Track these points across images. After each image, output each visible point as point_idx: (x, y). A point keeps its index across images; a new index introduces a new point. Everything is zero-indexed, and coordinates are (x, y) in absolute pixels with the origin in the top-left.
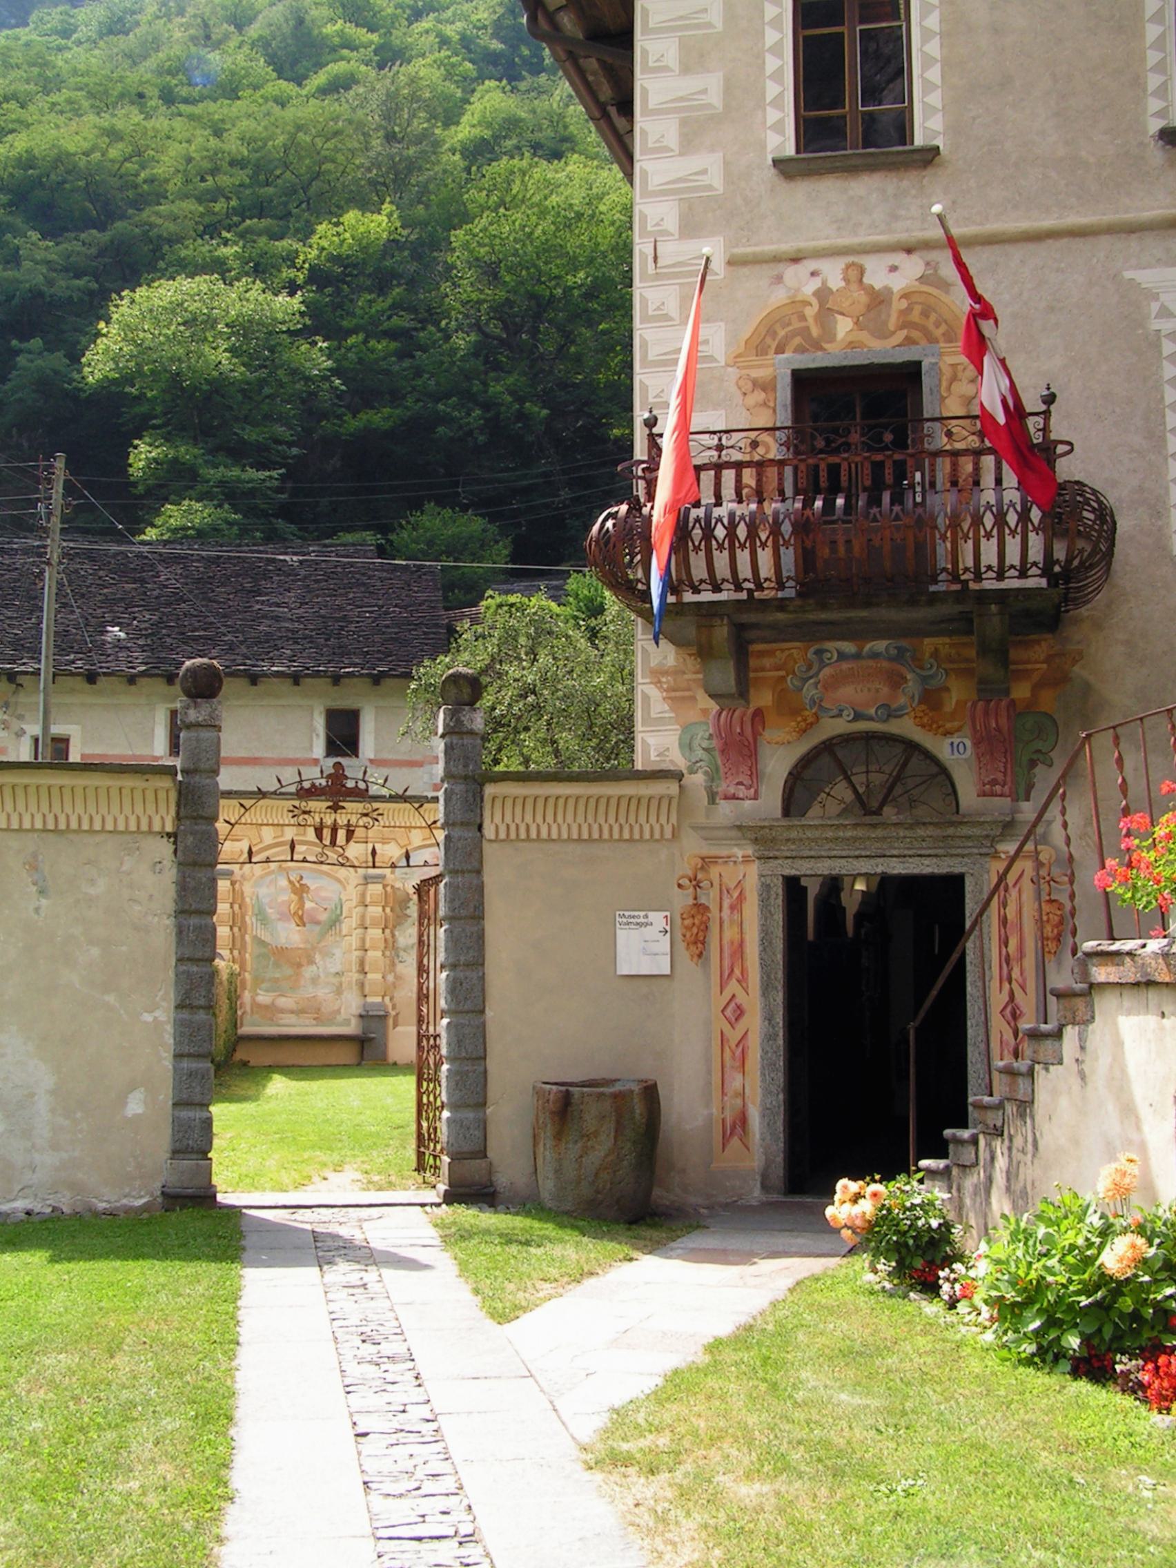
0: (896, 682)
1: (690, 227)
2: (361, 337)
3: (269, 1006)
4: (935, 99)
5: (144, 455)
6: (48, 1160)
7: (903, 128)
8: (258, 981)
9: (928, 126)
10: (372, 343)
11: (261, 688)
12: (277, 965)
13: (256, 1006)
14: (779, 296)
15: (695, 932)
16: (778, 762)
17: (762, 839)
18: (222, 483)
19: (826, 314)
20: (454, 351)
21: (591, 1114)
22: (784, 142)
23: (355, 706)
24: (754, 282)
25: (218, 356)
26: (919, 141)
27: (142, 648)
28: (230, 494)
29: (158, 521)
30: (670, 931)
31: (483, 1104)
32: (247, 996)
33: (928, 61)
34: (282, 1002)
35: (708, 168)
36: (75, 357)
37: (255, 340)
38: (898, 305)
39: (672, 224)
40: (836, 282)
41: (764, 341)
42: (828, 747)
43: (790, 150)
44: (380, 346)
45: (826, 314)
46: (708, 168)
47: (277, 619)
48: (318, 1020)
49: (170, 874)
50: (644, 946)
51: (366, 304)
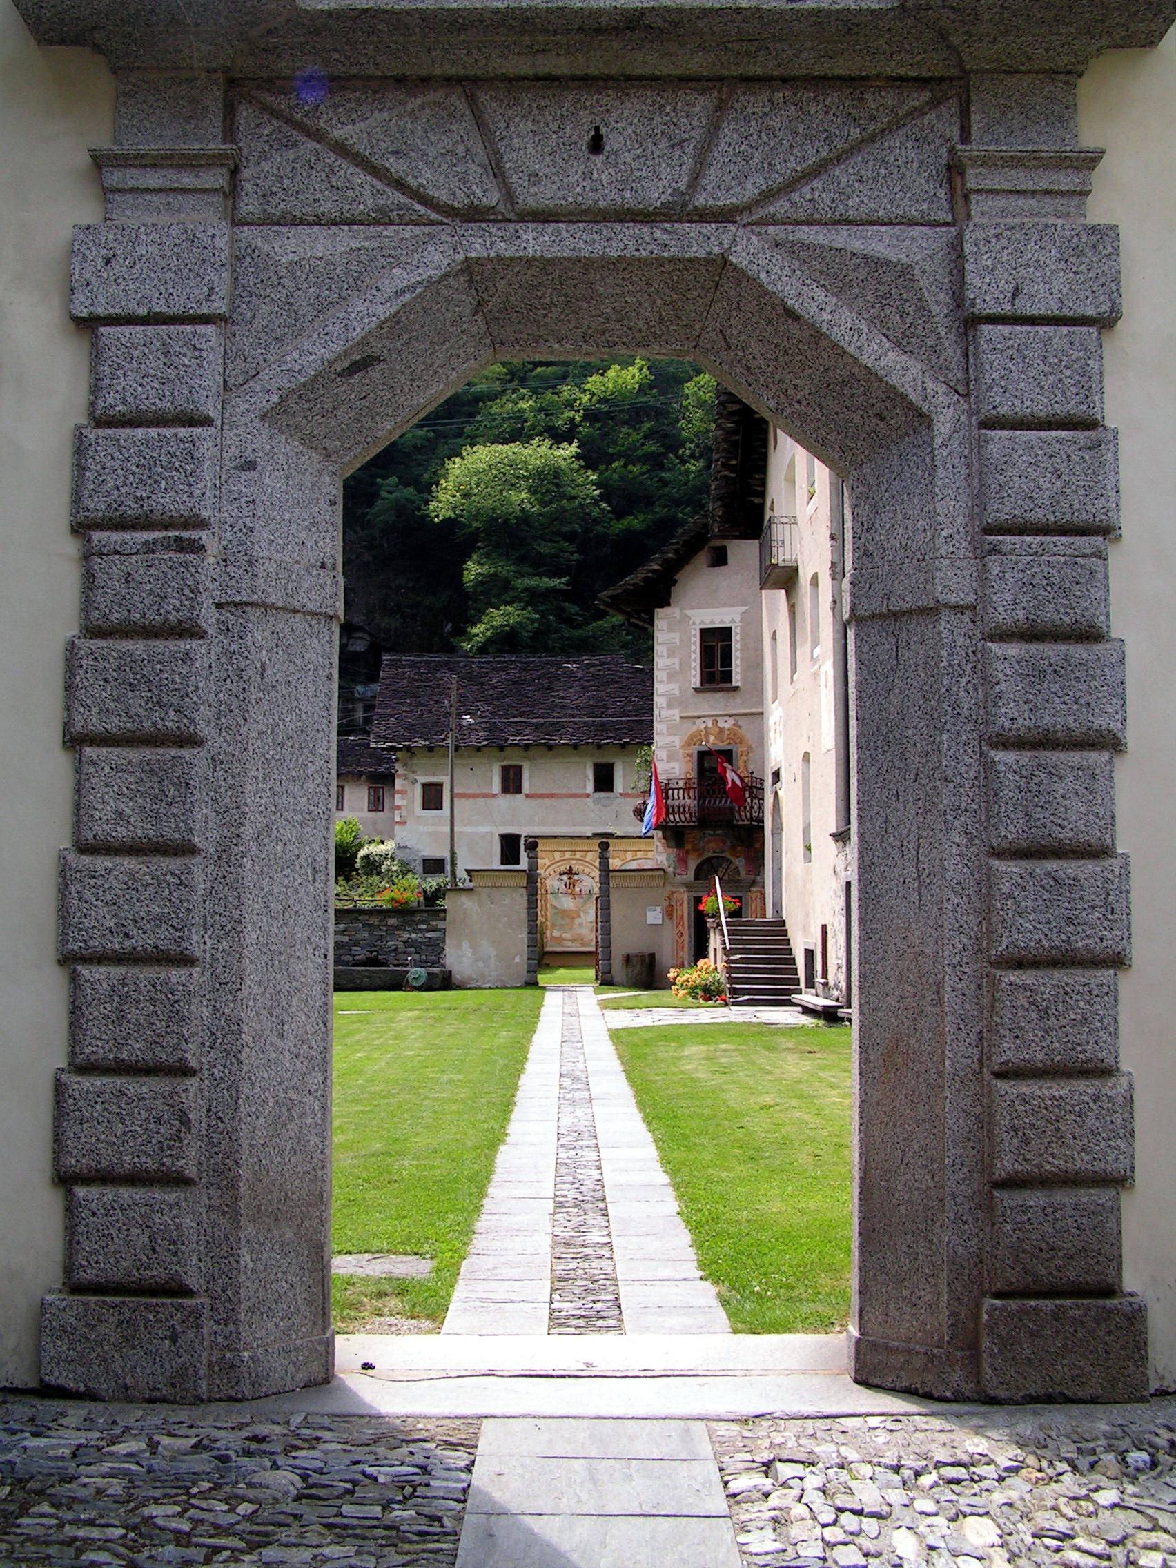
0: (724, 842)
1: (669, 707)
2: (622, 462)
3: (559, 937)
4: (738, 670)
5: (473, 570)
6: (494, 974)
7: (727, 677)
8: (553, 925)
9: (737, 680)
10: (630, 467)
11: (554, 752)
12: (562, 918)
13: (553, 937)
14: (694, 728)
15: (669, 912)
16: (692, 865)
17: (688, 886)
18: (526, 589)
19: (707, 735)
20: (687, 472)
21: (634, 961)
22: (696, 681)
23: (612, 761)
24: (688, 724)
25: (520, 498)
26: (734, 684)
27: (484, 730)
28: (534, 597)
29: (485, 619)
30: (662, 912)
31: (609, 959)
32: (548, 933)
33: (737, 658)
34: (564, 936)
35: (675, 688)
36: (426, 489)
37: (548, 482)
38: (727, 732)
39: (664, 705)
40: (710, 725)
41: (690, 742)
42: (709, 860)
43: (698, 685)
44: (635, 469)
45: (707, 735)
46: (675, 688)
47: (563, 707)
48: (583, 945)
49: (526, 898)
50: (654, 916)
51: (628, 436)
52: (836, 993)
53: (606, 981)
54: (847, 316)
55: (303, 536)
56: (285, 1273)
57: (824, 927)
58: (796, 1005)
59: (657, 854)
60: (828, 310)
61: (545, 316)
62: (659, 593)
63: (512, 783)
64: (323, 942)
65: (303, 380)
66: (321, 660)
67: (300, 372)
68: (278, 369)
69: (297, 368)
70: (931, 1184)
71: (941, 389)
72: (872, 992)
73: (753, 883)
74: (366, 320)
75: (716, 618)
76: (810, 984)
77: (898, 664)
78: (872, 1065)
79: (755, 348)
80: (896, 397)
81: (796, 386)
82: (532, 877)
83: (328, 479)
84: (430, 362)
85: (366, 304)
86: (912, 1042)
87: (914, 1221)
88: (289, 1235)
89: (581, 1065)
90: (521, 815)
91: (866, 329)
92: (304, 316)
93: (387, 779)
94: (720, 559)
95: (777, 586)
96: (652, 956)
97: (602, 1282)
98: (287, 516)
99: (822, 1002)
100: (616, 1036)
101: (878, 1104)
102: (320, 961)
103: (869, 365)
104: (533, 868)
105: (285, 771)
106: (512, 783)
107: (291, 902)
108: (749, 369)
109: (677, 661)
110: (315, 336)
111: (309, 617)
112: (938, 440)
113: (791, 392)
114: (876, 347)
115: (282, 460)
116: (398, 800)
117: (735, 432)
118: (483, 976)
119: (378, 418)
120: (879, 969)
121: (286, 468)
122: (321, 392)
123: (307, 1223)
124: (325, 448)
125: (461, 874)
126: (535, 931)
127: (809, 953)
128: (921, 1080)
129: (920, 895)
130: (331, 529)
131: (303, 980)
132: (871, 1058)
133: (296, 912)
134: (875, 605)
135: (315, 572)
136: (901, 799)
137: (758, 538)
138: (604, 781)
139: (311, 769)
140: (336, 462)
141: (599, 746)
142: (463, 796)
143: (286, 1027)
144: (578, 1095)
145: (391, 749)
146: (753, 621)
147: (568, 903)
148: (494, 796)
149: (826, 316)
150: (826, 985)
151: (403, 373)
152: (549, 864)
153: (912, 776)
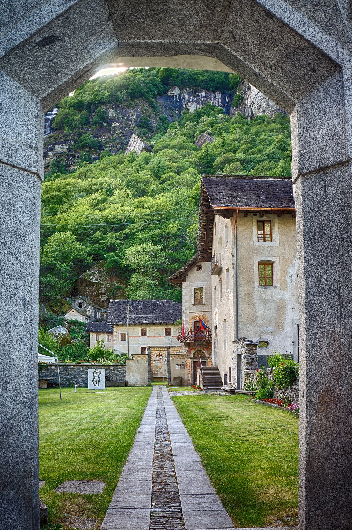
1: (186, 309)
16: (193, 352)
24: (191, 314)
52: (234, 386)
53: (170, 385)
54: (297, 16)
55: (19, 129)
56: (10, 514)
57: (230, 368)
58: (222, 390)
59: (184, 350)
60: (288, 12)
61: (143, 23)
62: (182, 278)
63: (144, 333)
64: (29, 341)
65: (17, 44)
66: (28, 195)
67: (16, 40)
68: (4, 39)
69: (14, 38)
70: (348, 464)
71: (346, 52)
72: (313, 365)
73: (209, 357)
74: (50, 14)
75: (198, 285)
76: (226, 383)
77: (326, 194)
78: (313, 403)
79: (249, 39)
80: (323, 56)
81: (269, 58)
82: (149, 356)
83: (34, 104)
84: (85, 45)
85: (51, 6)
86: (337, 390)
87: (337, 484)
88: (12, 494)
89: (163, 407)
90: (146, 342)
91: (307, 22)
92: (18, 12)
93: (111, 333)
94: (200, 268)
95: (216, 274)
96: (182, 377)
97: (173, 495)
98: (10, 117)
99: (230, 389)
100: (172, 398)
101: (316, 423)
102: (28, 351)
103: (309, 39)
104: (149, 353)
105: (7, 249)
106: (144, 333)
107: (11, 319)
108: (245, 52)
109: (188, 297)
110: (24, 22)
111: (22, 171)
112: (345, 77)
113: (267, 62)
114: (312, 31)
115: (7, 88)
116: (114, 338)
117: (204, 231)
118: (136, 383)
119: (59, 74)
120: (317, 353)
121: (10, 93)
122: (27, 53)
123: (22, 487)
124: (32, 88)
125: (130, 355)
126: (150, 371)
127: (226, 376)
128: (342, 410)
129: (341, 313)
130: (35, 129)
131: (18, 361)
132: (313, 399)
133: (14, 325)
134: (313, 166)
135: (25, 148)
136: (329, 264)
137: (210, 262)
138: (168, 333)
139: (22, 250)
140: (38, 97)
141: (167, 324)
142: (131, 337)
143: (8, 386)
144: (162, 416)
145: (112, 324)
146: (209, 286)
147: (159, 364)
148: (139, 337)
149: (286, 15)
150: (231, 384)
151: (71, 49)
152: (154, 353)
153: (335, 251)
